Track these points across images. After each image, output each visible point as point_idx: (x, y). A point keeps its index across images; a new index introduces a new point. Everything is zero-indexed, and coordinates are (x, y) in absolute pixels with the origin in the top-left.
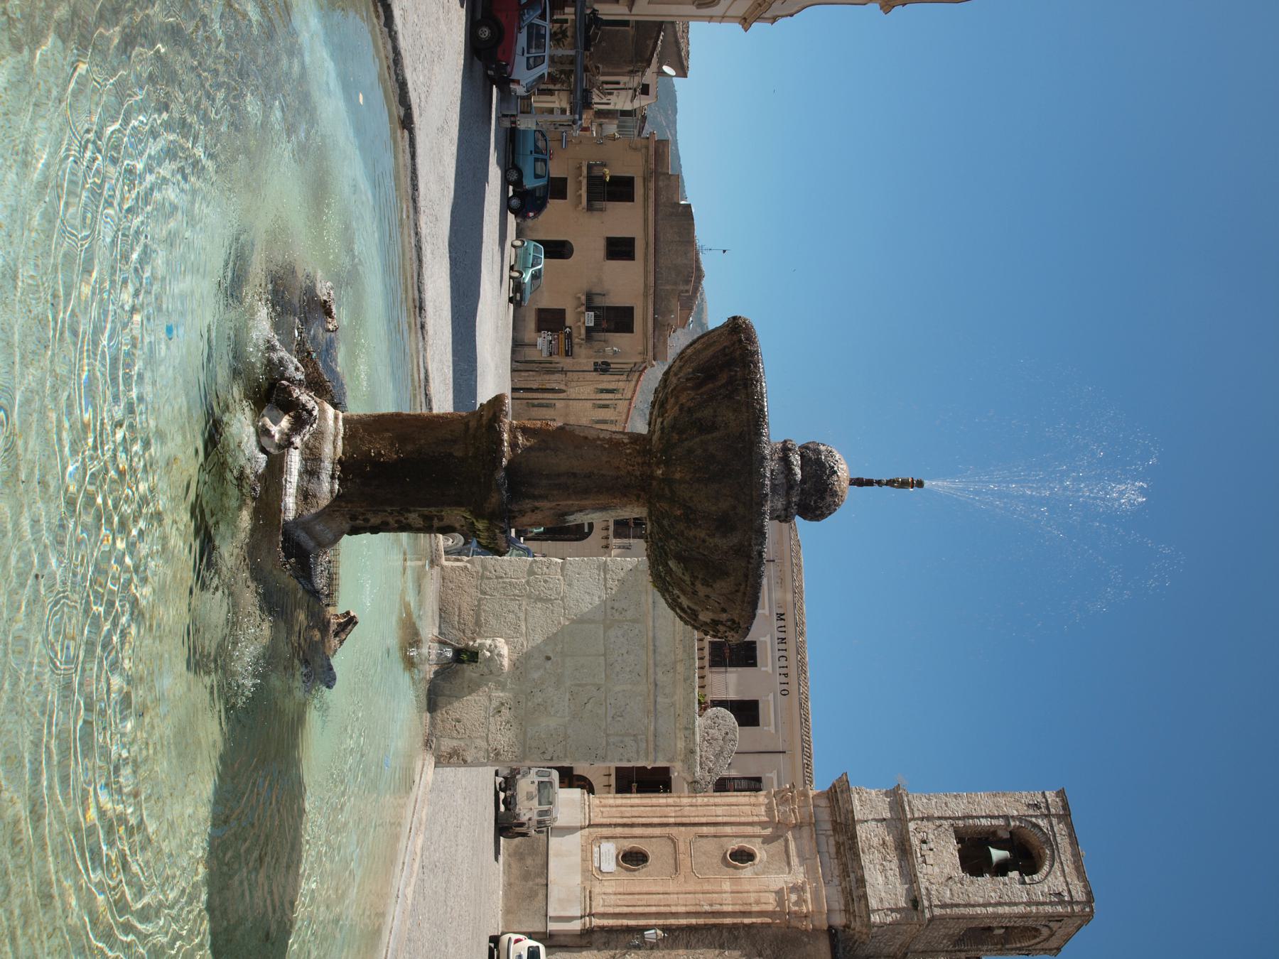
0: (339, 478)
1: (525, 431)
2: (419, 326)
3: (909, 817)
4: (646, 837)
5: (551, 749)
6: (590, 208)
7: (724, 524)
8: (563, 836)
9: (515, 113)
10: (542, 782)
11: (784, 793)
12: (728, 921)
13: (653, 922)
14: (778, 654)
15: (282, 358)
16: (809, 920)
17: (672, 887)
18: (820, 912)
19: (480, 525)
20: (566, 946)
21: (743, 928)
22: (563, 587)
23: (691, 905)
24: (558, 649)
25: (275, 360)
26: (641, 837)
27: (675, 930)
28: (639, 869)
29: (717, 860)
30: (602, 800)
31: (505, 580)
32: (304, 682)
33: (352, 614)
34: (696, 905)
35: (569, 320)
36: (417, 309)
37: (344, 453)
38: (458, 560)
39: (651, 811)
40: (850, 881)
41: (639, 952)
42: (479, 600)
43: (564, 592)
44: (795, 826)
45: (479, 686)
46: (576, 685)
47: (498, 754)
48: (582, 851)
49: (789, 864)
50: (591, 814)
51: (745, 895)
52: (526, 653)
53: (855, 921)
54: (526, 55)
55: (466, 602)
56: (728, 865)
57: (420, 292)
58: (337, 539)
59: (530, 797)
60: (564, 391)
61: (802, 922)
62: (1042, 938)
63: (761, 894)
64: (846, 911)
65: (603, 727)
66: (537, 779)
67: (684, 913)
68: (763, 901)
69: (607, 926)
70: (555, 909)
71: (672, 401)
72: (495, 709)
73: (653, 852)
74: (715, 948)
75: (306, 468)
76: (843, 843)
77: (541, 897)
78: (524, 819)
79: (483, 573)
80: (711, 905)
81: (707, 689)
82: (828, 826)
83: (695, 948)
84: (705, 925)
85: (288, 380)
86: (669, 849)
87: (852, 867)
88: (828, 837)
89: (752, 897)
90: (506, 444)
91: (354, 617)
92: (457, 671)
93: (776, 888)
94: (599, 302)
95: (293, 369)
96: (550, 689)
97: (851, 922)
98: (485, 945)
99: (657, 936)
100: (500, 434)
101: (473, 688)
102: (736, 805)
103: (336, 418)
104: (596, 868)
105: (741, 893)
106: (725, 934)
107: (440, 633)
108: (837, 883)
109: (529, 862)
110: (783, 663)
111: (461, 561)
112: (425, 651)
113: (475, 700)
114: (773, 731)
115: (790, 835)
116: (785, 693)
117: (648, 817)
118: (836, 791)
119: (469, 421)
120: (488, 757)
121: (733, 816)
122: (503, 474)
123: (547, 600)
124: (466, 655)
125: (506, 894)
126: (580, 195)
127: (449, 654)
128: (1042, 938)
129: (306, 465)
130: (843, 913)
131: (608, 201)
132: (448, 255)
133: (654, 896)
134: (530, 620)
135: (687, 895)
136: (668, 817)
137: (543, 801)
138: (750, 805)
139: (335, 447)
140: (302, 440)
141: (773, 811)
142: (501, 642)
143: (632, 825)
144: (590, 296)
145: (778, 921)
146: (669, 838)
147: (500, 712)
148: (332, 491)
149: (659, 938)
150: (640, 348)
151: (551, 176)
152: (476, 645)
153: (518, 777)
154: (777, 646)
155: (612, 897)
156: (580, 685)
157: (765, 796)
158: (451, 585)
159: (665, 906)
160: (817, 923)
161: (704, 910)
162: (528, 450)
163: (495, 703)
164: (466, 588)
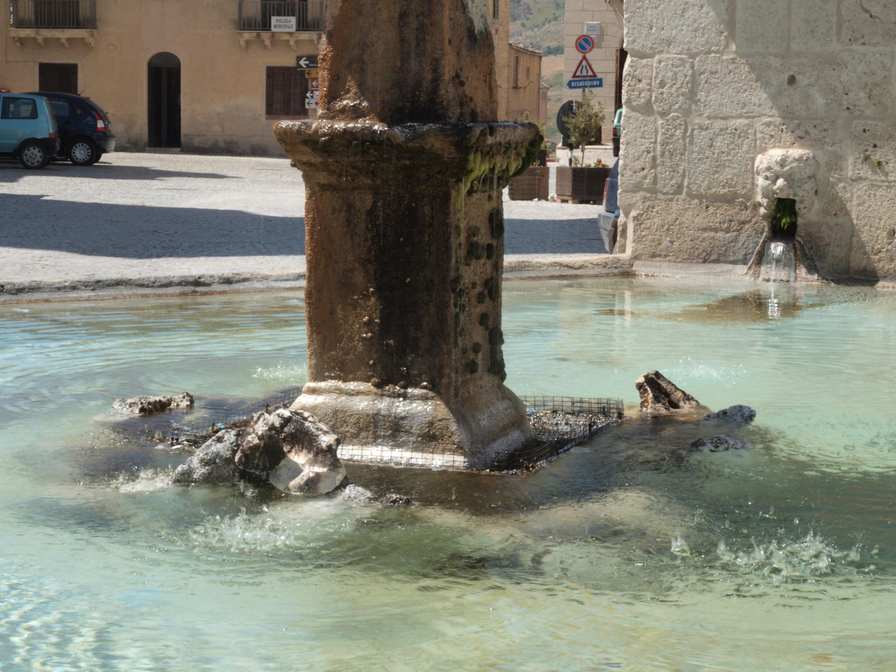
0: (405, 387)
2: (226, 287)
6: (90, 23)
15: (202, 460)
22: (672, 55)
24: (775, 62)
25: (204, 471)
31: (658, 153)
32: (727, 449)
33: (641, 380)
35: (286, 60)
36: (199, 289)
37: (367, 380)
43: (681, 53)
45: (835, 198)
46: (839, 33)
52: (784, 118)
57: (169, 284)
72: (875, 172)
75: (389, 436)
79: (648, 190)
85: (234, 452)
90: (351, 125)
91: (646, 377)
92: (809, 234)
95: (219, 446)
100: (334, 136)
103: (313, 391)
107: (744, 262)
112: (772, 288)
113: (859, 205)
119: (318, 184)
122: (397, 130)
123: (694, 82)
126: (69, 40)
127: (777, 248)
129: (384, 437)
132: (154, 260)
134: (726, 111)
139: (359, 393)
140: (326, 433)
142: (762, 161)
144: (245, 24)
147: (879, 164)
148: (425, 398)
151: (37, 90)
152: (765, 201)
158: (665, 243)
163: (866, 171)
164: (670, 218)
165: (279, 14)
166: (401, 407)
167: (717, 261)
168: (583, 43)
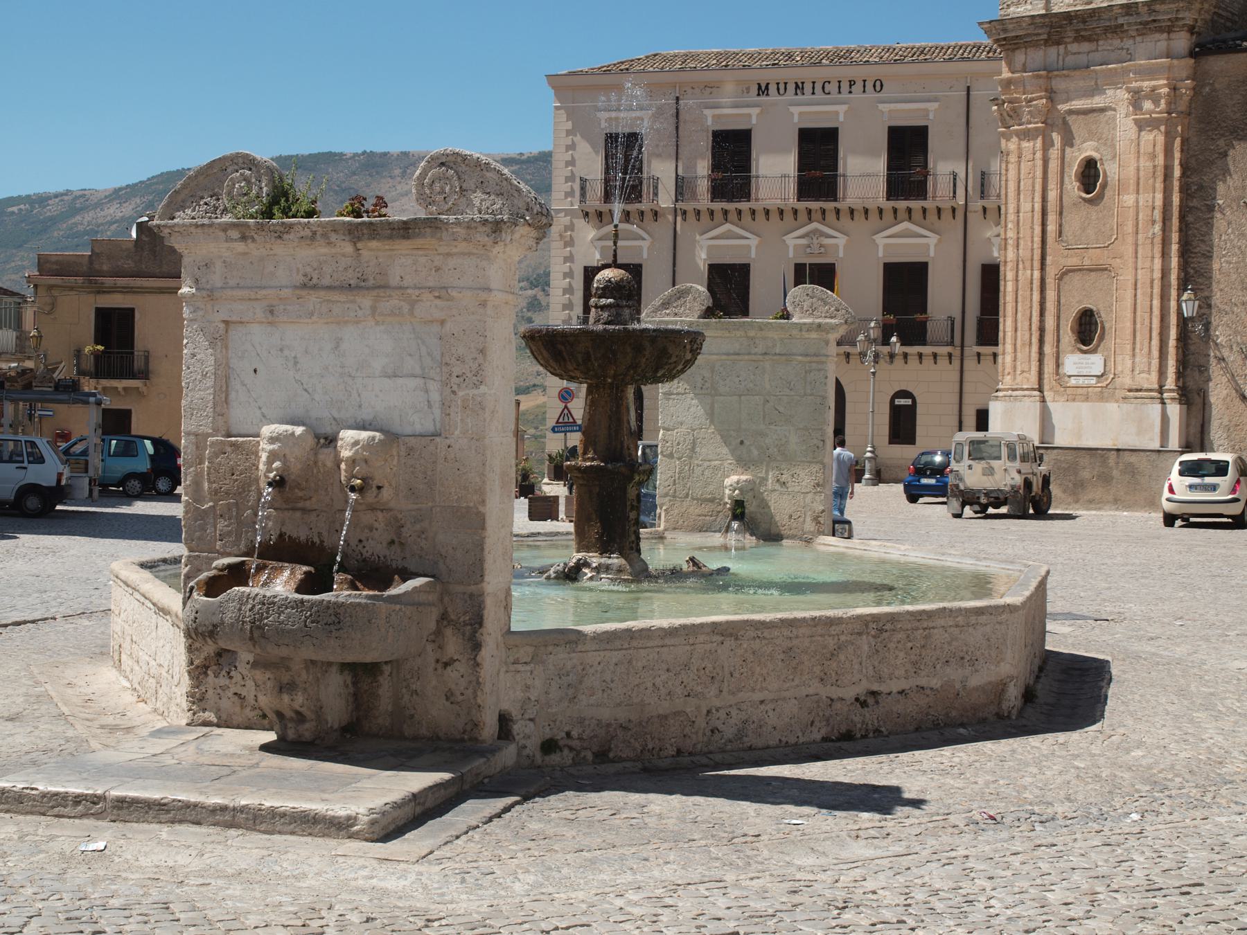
1: (585, 453)
4: (1059, 310)
5: (815, 441)
6: (144, 375)
7: (639, 349)
8: (1053, 427)
9: (87, 480)
10: (970, 455)
11: (1005, 114)
12: (1176, 199)
13: (1173, 304)
14: (819, 95)
16: (1179, 84)
17: (1127, 277)
18: (1170, 68)
19: (637, 478)
20: (1203, 426)
21: (1188, 177)
23: (1152, 250)
26: (1058, 317)
27: (1187, 273)
28: (1102, 322)
29: (1093, 212)
30: (1006, 372)
34: (1152, 243)
38: (660, 517)
39: (1023, 302)
40: (1129, 25)
41: (1214, 323)
42: (693, 499)
44: (1050, 99)
45: (763, 500)
47: (818, 485)
48: (1074, 400)
49: (1102, 110)
50: (1025, 387)
51: (1142, 173)
53: (1183, 19)
54: (26, 464)
55: (695, 510)
56: (1100, 197)
58: (642, 560)
59: (990, 472)
61: (1182, 95)
63: (1142, 151)
64: (1169, 30)
65: (798, 398)
66: (966, 461)
67: (1163, 261)
68: (1151, 150)
69: (1178, 368)
70: (1152, 440)
71: (571, 374)
73: (1080, 302)
74: (1212, 218)
76: (1077, 31)
77: (1133, 458)
78: (1018, 480)
80: (1154, 222)
81: (872, 205)
82: (1052, 52)
83: (1212, 246)
84: (1181, 230)
86: (1076, 279)
87: (1110, 20)
88: (1067, 53)
89: (1145, 164)
93: (1135, 129)
97: (1184, 25)
98: (1178, 532)
99: (1190, 300)
101: (764, 505)
102: (1019, 182)
104: (1098, 382)
105: (1139, 179)
106: (1195, 203)
108: (1131, 42)
109: (1086, 474)
110: (830, 88)
111: (660, 514)
114: (936, 105)
115: (1063, 107)
116: (879, 85)
117: (1031, 307)
118: (1005, 39)
120: (820, 492)
121: (1033, 187)
122: (609, 465)
123: (694, 443)
124: (739, 511)
125: (1128, 507)
126: (125, 389)
127: (735, 525)
130: (1173, 35)
131: (132, 347)
133: (1138, 301)
134: (710, 457)
135: (1139, 255)
136: (1032, 280)
137: (996, 454)
138: (1019, 163)
141: (1029, 130)
142: (728, 482)
143: (1042, 330)
145: (1179, 128)
146: (1060, 279)
149: (1193, 297)
153: (962, 487)
154: (808, 96)
155: (1137, 360)
156: (764, 417)
157: (1008, 140)
158: (681, 522)
159: (1152, 287)
160: (1184, 75)
161: (1161, 233)
162: (595, 452)
163: (777, 487)
166: (610, 561)
167: (706, 531)
168: (567, 396)
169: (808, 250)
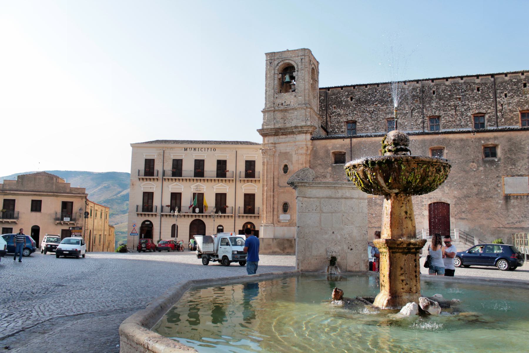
3: (273, 109)
5: (364, 232)
6: (17, 218)
60: (90, 231)
62: (314, 67)
64: (306, 133)
65: (356, 214)
88: (279, 138)
94: (59, 216)
96: (344, 232)
109: (286, 245)
126: (11, 222)
128: (314, 67)
130: (307, 135)
150: (80, 199)
155: (274, 217)
156: (342, 222)
165: (66, 217)
169: (197, 190)
